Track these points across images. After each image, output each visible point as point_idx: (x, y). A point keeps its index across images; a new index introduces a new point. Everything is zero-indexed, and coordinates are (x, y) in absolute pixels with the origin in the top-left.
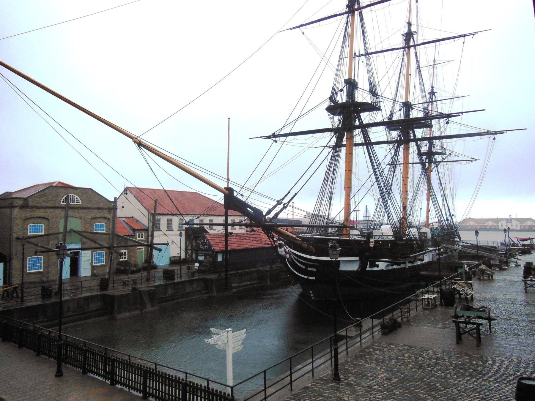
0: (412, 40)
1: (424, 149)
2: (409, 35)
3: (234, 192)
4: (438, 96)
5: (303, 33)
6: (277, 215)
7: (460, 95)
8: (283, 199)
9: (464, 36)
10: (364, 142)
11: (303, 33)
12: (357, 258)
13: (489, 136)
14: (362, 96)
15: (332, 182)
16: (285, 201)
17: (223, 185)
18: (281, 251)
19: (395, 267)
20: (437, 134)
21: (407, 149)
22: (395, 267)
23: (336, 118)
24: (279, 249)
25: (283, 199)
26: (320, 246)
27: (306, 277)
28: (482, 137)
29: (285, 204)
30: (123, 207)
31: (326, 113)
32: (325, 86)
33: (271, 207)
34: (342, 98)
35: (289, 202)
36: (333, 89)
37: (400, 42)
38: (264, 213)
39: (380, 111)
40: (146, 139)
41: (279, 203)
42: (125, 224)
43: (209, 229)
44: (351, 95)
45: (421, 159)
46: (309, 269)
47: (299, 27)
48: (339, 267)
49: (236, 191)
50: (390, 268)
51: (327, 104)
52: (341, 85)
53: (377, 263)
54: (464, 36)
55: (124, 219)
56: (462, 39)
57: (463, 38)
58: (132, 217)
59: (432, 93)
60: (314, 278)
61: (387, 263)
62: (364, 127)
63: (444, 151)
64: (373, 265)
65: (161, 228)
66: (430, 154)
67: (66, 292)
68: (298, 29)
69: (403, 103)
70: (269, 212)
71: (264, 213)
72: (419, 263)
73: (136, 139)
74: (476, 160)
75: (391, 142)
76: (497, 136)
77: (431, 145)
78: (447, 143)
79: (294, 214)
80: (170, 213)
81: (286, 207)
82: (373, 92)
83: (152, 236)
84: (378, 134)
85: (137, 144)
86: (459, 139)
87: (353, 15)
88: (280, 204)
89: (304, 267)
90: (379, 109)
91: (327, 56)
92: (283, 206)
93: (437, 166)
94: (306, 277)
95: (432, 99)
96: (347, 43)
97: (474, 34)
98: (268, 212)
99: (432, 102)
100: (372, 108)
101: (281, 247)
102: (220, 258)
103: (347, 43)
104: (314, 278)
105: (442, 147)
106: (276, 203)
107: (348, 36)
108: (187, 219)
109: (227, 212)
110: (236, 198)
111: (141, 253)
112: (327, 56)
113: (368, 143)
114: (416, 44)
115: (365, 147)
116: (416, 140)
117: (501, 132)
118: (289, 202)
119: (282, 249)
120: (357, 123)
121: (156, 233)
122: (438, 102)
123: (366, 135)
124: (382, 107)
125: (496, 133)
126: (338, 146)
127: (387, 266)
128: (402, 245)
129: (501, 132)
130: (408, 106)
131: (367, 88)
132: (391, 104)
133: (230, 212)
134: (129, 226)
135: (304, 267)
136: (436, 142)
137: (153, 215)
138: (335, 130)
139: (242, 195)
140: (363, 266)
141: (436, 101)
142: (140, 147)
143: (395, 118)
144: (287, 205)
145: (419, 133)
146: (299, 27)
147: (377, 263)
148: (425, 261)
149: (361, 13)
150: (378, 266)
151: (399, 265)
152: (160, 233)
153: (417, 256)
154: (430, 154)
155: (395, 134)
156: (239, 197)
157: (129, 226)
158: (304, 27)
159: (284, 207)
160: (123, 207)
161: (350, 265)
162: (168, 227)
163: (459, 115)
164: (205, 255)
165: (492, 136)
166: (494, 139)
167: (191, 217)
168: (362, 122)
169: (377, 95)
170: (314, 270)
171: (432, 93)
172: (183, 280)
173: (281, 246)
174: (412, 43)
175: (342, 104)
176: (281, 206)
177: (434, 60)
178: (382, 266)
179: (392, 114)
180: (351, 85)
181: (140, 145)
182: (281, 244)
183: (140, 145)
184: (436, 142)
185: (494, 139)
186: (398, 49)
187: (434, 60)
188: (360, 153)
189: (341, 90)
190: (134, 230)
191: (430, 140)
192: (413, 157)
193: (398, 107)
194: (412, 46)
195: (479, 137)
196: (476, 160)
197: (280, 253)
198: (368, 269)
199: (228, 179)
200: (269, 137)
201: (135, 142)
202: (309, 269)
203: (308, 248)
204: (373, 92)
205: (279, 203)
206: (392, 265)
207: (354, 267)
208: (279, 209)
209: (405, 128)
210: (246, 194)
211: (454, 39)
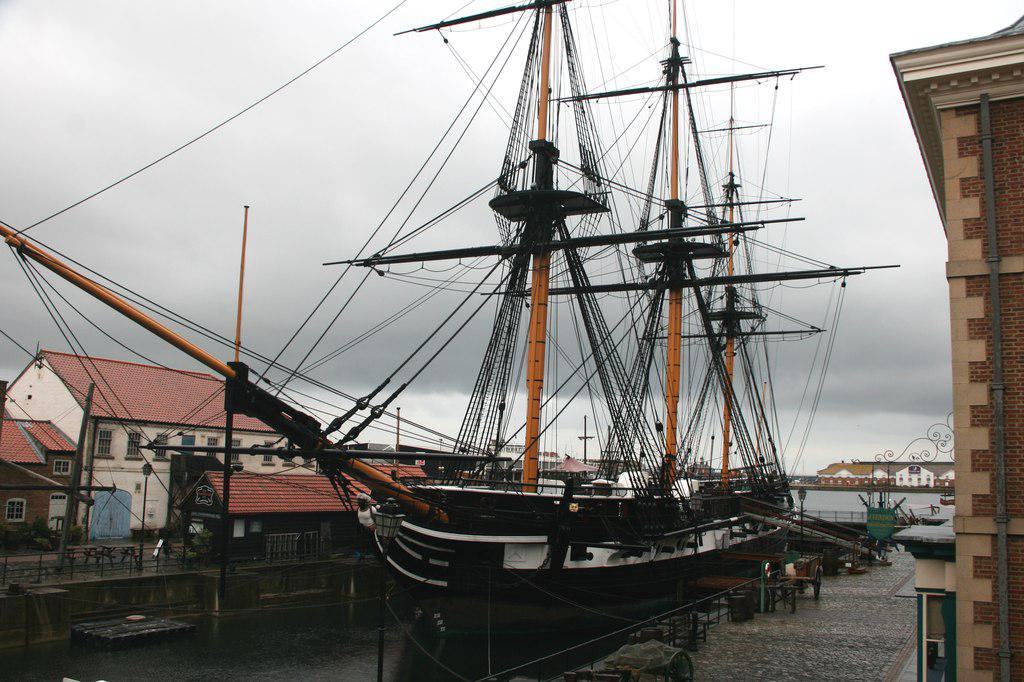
0: (680, 74)
1: (719, 305)
2: (674, 65)
3: (250, 373)
4: (746, 193)
5: (446, 41)
6: (355, 432)
7: (786, 197)
8: (371, 397)
9: (777, 74)
10: (572, 285)
11: (446, 41)
12: (543, 539)
13: (833, 278)
14: (567, 179)
15: (507, 356)
16: (377, 401)
17: (224, 356)
18: (365, 516)
19: (632, 560)
20: (740, 270)
21: (677, 301)
22: (632, 560)
23: (514, 225)
24: (360, 514)
25: (371, 397)
26: (463, 512)
27: (422, 579)
28: (822, 279)
29: (374, 408)
30: (30, 397)
31: (491, 213)
32: (487, 150)
33: (341, 414)
34: (525, 181)
35: (385, 405)
36: (507, 161)
37: (655, 76)
38: (324, 427)
39: (605, 215)
40: (38, 238)
41: (361, 405)
42: (29, 440)
43: (155, 460)
44: (545, 174)
45: (708, 327)
46: (432, 561)
47: (437, 27)
48: (501, 559)
49: (254, 372)
50: (621, 562)
51: (493, 192)
52: (523, 153)
53: (589, 550)
54: (777, 74)
55: (27, 425)
56: (773, 80)
57: (775, 78)
58: (49, 422)
59: (731, 188)
60: (445, 584)
61: (614, 551)
62: (571, 245)
63: (757, 311)
64: (581, 554)
65: (113, 452)
66: (731, 317)
67: (650, 449)
68: (435, 31)
69: (666, 202)
70: (337, 424)
71: (324, 427)
72: (689, 552)
73: (15, 236)
74: (819, 331)
75: (644, 287)
76: (848, 279)
77: (732, 296)
78: (766, 292)
79: (396, 430)
80: (27, 418)
81: (378, 416)
82: (589, 171)
83: (91, 469)
84: (602, 267)
85: (15, 249)
86: (777, 282)
87: (549, 12)
88: (363, 407)
89: (419, 557)
90: (602, 208)
91: (488, 82)
92: (372, 412)
93: (744, 343)
94: (422, 579)
95: (731, 199)
96: (536, 67)
97: (794, 72)
98: (334, 423)
99: (732, 205)
100: (590, 204)
101: (363, 508)
102: (239, 532)
103: (536, 67)
104: (445, 584)
105: (755, 304)
106: (354, 404)
107: (538, 52)
108: (151, 434)
109: (230, 421)
110: (253, 386)
111: (58, 508)
112: (488, 82)
113: (582, 289)
114: (689, 82)
115: (574, 296)
116: (696, 284)
117: (856, 272)
118: (385, 405)
119: (367, 513)
120: (557, 237)
121: (99, 463)
122: (743, 207)
123: (575, 266)
124: (610, 203)
125: (846, 273)
126: (514, 289)
127: (612, 558)
128: (653, 514)
129: (856, 272)
130: (677, 209)
131: (578, 162)
132: (643, 203)
133: (240, 420)
134: (37, 442)
135: (419, 557)
136: (744, 290)
137: (91, 421)
138: (503, 252)
139: (267, 381)
140: (556, 557)
141: (739, 204)
142: (24, 259)
143: (654, 227)
144: (381, 412)
145: (703, 267)
146: (437, 27)
147: (589, 550)
148: (701, 550)
149: (565, 8)
150: (590, 557)
151: (640, 555)
152: (111, 463)
153: (683, 534)
154: (731, 317)
155: (650, 268)
156: (263, 385)
157: (37, 442)
158: (448, 28)
159: (375, 415)
160: (30, 397)
161: (526, 556)
162: (129, 451)
163: (860, 273)
164: (206, 523)
165: (840, 280)
166: (844, 285)
167: (161, 431)
168: (568, 235)
169: (599, 178)
170: (447, 564)
171: (731, 188)
172: (145, 574)
173: (364, 505)
174: (681, 81)
175: (524, 194)
176: (367, 412)
177: (732, 120)
178: (600, 557)
179: (645, 223)
180: (546, 153)
181: (23, 250)
182: (365, 500)
183: (23, 250)
184: (744, 290)
185: (844, 285)
186: (653, 90)
187: (732, 120)
188: (563, 310)
189: (523, 165)
190: (49, 453)
191: (730, 280)
192: (693, 323)
193: (657, 210)
194: (682, 86)
195: (814, 281)
196: (819, 331)
197: (361, 521)
198: (569, 564)
199: (238, 344)
200: (367, 263)
201: (10, 243)
202: (432, 561)
203: (431, 512)
204: (589, 171)
205: (361, 405)
206: (625, 556)
207: (533, 561)
208: (362, 420)
209: (672, 252)
210: (275, 376)
211: (760, 80)
